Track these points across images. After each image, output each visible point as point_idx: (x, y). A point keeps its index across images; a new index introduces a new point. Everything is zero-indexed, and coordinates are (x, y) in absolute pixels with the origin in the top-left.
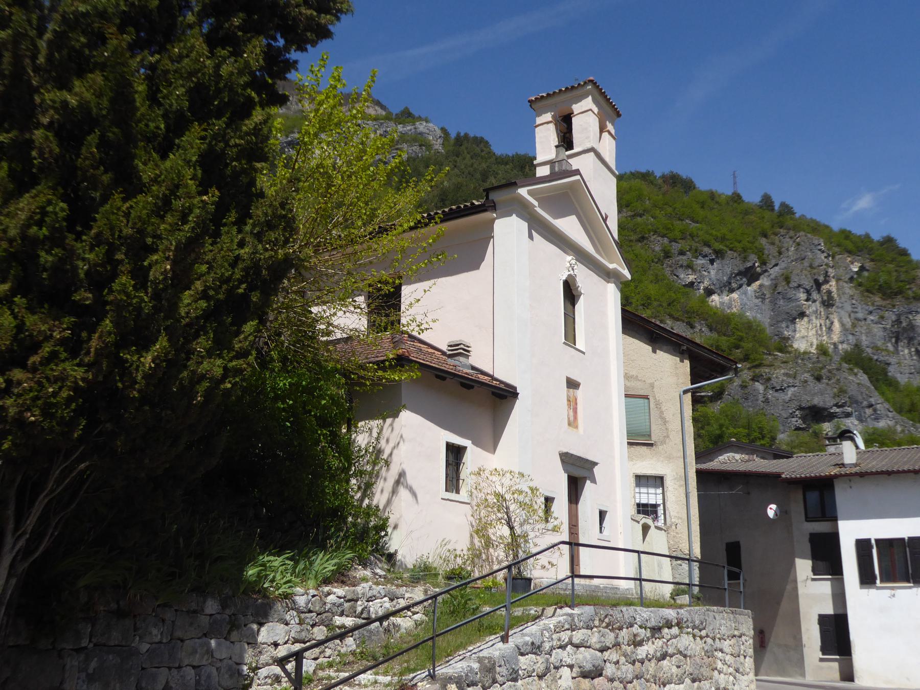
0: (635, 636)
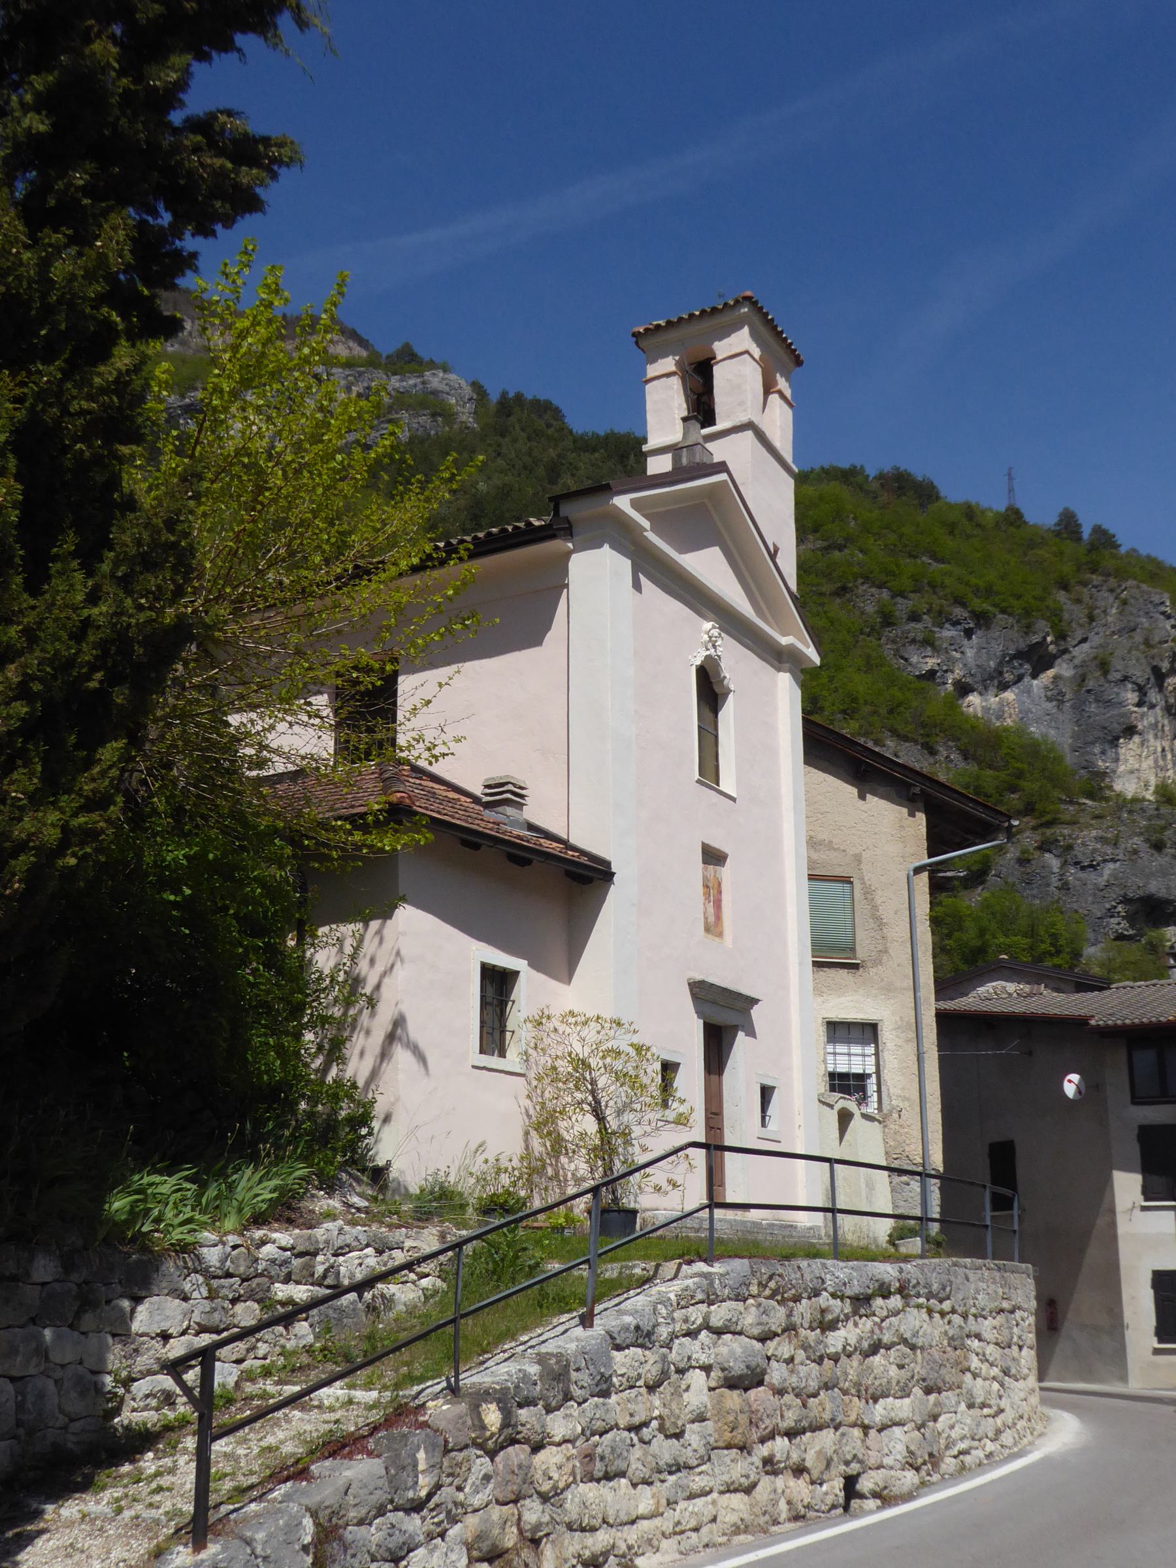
0: (823, 1311)
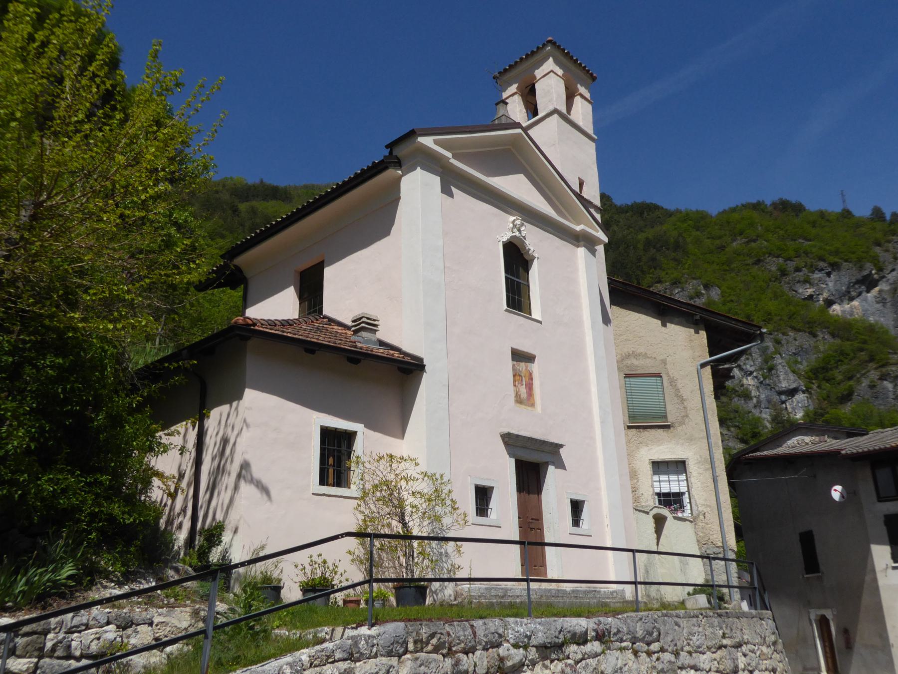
0: (502, 659)
